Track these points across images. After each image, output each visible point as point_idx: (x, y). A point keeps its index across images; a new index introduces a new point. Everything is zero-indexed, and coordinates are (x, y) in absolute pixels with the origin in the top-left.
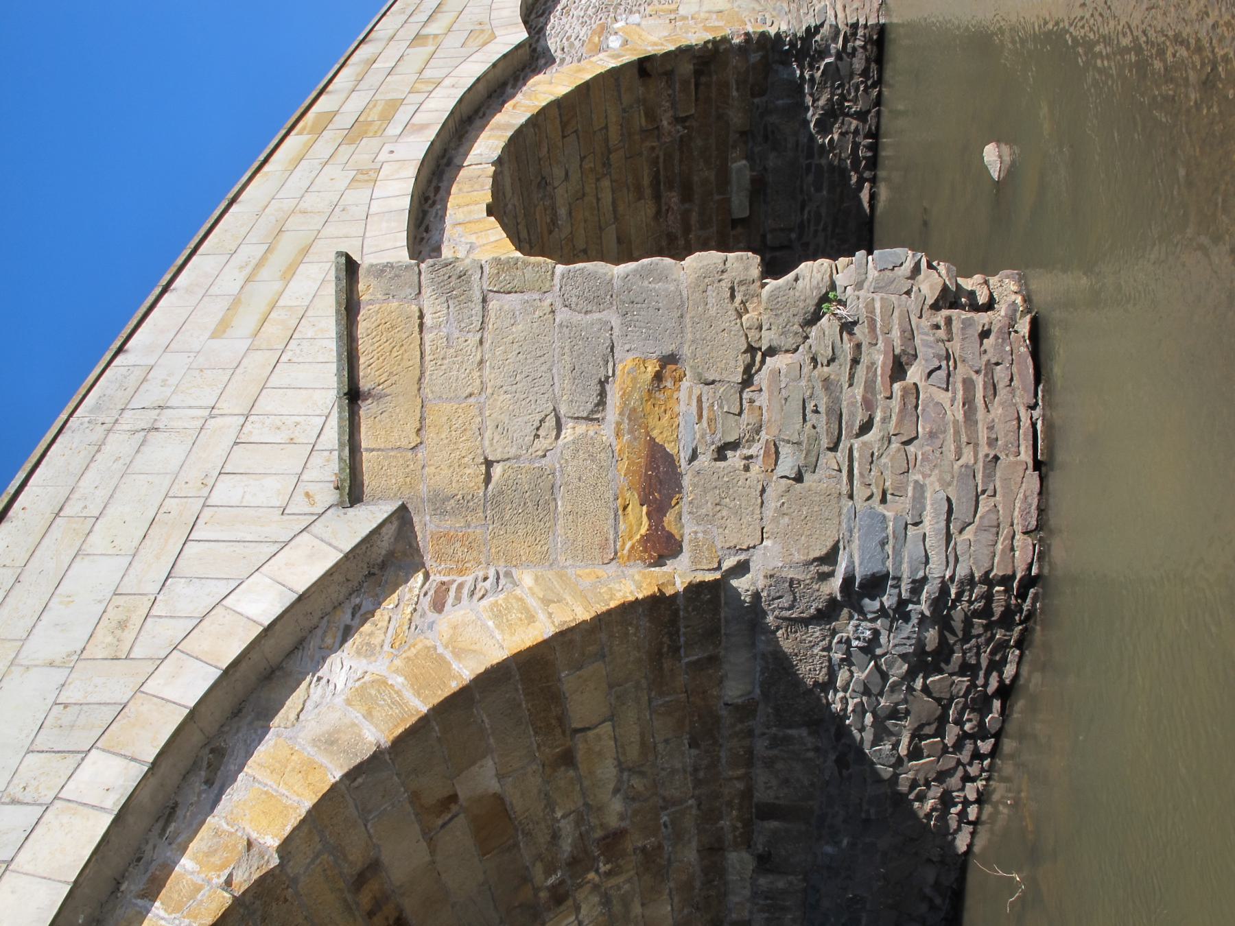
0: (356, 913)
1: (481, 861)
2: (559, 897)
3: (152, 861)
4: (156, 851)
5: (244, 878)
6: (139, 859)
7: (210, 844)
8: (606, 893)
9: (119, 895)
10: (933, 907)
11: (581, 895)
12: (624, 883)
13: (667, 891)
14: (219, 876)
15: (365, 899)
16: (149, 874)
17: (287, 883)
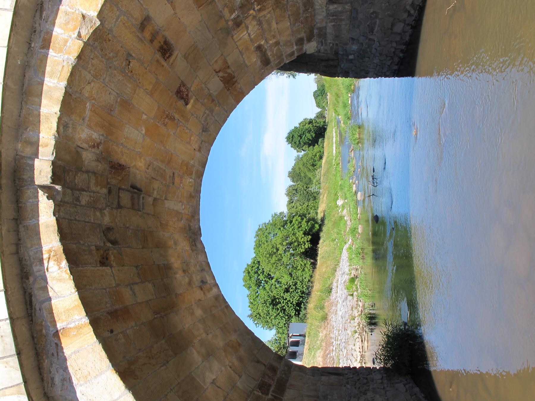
0: (145, 41)
1: (198, 11)
2: (238, 24)
3: (41, 31)
4: (41, 27)
5: (86, 33)
6: (35, 31)
7: (65, 19)
8: (259, 20)
9: (32, 49)
10: (410, 15)
11: (248, 22)
12: (267, 14)
13: (288, 16)
14: (74, 34)
15: (147, 34)
16: (42, 38)
17: (107, 32)
